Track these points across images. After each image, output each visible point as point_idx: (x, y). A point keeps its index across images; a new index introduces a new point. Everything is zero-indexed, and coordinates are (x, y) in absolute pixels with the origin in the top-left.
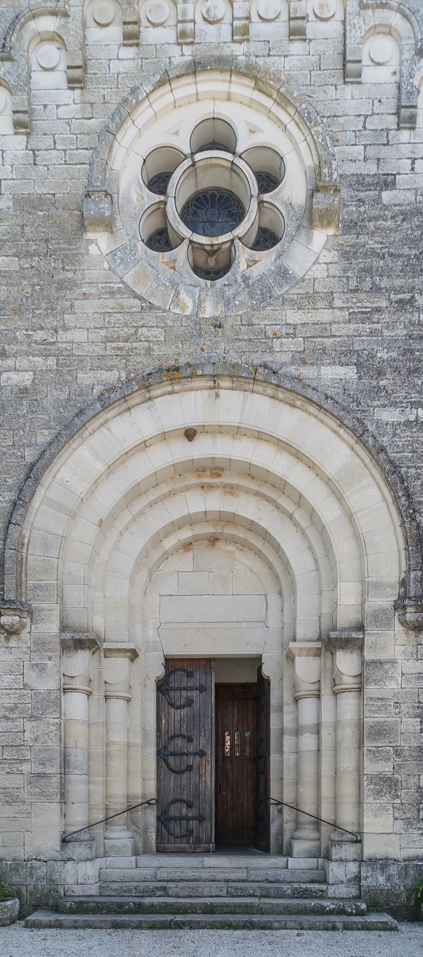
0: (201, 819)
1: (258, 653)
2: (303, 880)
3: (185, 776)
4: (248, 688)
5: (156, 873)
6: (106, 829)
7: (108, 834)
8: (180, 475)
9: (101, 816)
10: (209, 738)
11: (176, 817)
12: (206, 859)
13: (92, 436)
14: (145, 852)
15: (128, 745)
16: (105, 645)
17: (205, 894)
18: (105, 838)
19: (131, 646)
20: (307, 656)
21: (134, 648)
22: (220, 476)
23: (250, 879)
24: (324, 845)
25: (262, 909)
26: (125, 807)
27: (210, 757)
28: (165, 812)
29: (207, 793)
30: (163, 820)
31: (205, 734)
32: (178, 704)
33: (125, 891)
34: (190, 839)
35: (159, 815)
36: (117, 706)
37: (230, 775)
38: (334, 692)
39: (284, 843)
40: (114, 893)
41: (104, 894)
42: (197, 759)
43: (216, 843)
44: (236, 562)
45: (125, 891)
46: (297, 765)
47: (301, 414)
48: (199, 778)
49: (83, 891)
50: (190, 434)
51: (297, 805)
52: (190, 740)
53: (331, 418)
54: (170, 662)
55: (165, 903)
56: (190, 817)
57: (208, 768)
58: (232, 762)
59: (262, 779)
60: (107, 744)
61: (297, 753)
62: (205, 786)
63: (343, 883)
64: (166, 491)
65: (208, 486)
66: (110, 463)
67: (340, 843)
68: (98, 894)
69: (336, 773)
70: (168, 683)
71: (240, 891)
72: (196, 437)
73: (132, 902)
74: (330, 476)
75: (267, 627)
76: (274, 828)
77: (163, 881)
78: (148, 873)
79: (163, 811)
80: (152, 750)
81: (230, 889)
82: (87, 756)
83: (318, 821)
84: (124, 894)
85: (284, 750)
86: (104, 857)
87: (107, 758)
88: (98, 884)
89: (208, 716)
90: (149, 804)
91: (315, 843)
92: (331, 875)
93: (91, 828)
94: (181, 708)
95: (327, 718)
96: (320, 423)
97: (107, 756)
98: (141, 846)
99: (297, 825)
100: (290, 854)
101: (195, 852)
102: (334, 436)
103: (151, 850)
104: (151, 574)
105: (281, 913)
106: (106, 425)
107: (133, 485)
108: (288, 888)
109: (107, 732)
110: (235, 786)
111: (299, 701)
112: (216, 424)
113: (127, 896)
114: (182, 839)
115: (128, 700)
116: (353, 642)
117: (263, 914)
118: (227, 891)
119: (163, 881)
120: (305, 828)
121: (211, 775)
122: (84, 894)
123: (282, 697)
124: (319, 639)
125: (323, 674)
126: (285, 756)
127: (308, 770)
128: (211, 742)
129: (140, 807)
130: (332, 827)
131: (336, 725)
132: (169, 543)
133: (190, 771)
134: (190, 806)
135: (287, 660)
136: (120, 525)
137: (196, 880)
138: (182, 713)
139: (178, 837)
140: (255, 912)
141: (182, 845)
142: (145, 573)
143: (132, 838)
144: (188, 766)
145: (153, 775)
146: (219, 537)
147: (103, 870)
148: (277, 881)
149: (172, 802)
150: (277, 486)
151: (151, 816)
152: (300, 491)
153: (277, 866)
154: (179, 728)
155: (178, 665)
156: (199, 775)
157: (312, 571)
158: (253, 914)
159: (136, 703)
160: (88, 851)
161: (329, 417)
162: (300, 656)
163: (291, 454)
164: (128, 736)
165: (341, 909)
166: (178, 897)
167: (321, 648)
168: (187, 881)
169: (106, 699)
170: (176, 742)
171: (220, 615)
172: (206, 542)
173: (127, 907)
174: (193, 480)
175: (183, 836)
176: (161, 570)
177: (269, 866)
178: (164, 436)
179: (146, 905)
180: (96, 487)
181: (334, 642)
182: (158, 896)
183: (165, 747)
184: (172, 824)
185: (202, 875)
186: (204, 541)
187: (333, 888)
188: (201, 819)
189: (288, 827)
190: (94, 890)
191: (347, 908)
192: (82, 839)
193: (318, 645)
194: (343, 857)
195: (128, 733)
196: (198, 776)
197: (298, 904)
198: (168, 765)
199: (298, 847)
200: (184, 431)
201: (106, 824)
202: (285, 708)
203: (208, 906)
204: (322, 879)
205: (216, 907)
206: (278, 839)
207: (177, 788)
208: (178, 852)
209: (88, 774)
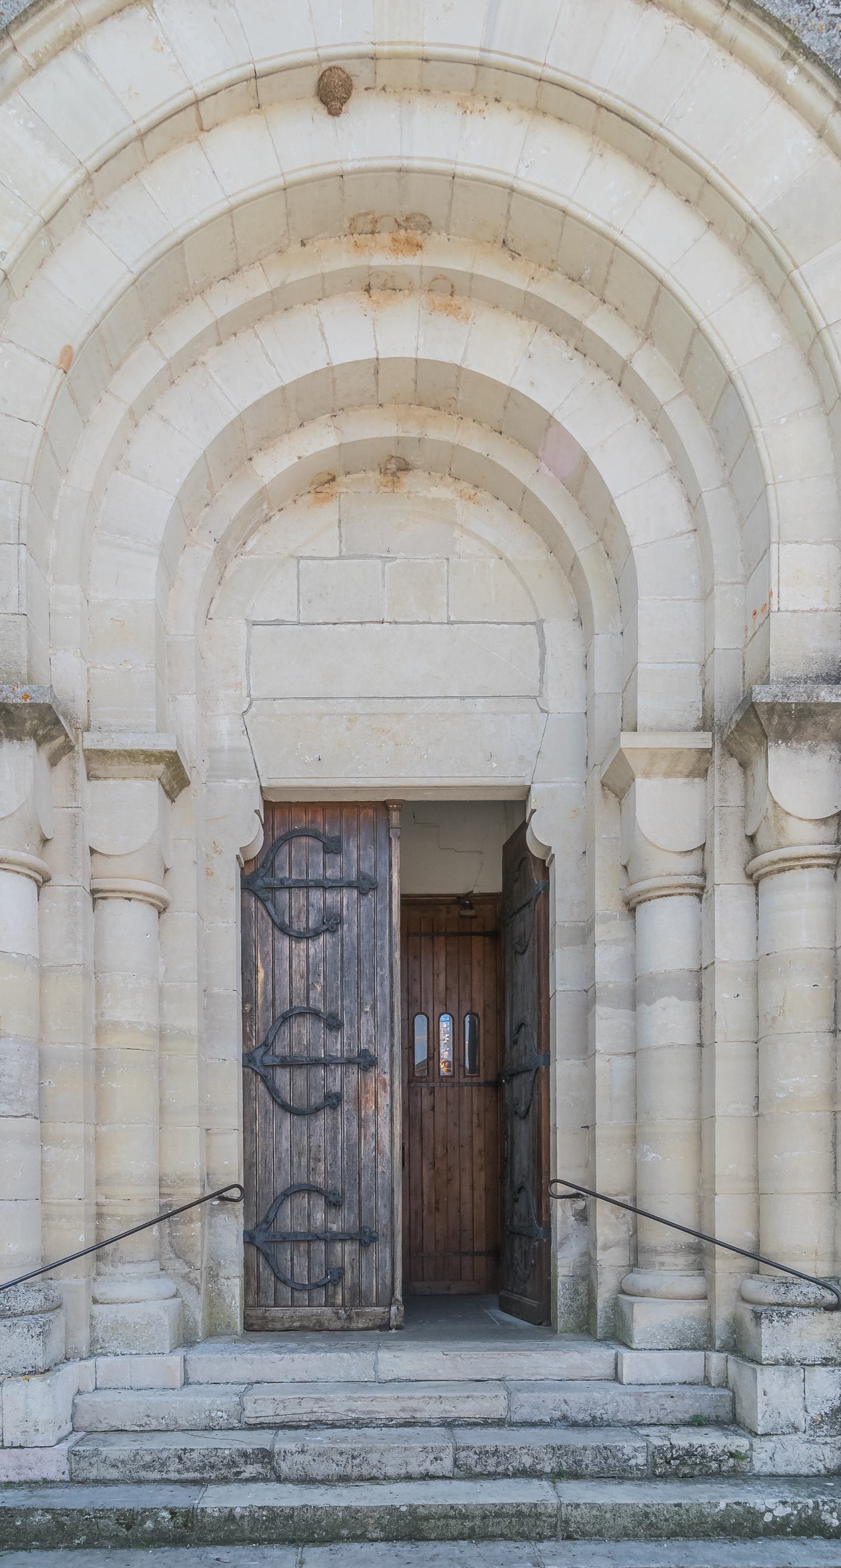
0: (364, 1238)
1: (517, 782)
2: (670, 1419)
3: (321, 1122)
4: (471, 907)
5: (240, 1403)
6: (99, 1274)
7: (102, 1289)
8: (303, 244)
9: (82, 1238)
10: (385, 1017)
11: (296, 1234)
12: (385, 1356)
13: (33, 80)
14: (212, 1334)
15: (162, 1035)
16: (90, 741)
17: (391, 1471)
18: (95, 1301)
19: (164, 744)
20: (668, 775)
21: (173, 748)
22: (420, 247)
23: (516, 1418)
24: (722, 1314)
25: (567, 1522)
26: (154, 1212)
27: (387, 1069)
28: (266, 1221)
29: (380, 1169)
30: (261, 1241)
31: (374, 1008)
32: (299, 925)
33: (146, 1467)
34: (335, 1293)
35: (250, 1228)
36: (128, 922)
37: (427, 1121)
38: (749, 876)
39: (600, 1305)
40: (114, 1474)
41: (83, 1475)
42: (354, 1075)
43: (405, 1302)
44: (457, 534)
45: (146, 1467)
46: (636, 1088)
47: (669, 23)
48: (359, 1126)
49: (20, 1467)
50: (333, 91)
51: (635, 1199)
52: (333, 1024)
53: (761, 33)
54: (277, 814)
55: (269, 1509)
56: (335, 1234)
57: (384, 1100)
58: (432, 1091)
59: (522, 1131)
60: (99, 1031)
61: (634, 1054)
62: (376, 1149)
63: (796, 1429)
64: (263, 289)
65: (384, 288)
66: (91, 165)
67: (784, 1310)
68: (66, 1477)
69: (757, 1107)
70: (272, 870)
71: (492, 1461)
72: (352, 104)
73: (165, 1508)
74: (754, 216)
75: (543, 711)
76: (565, 1263)
77: (261, 1426)
78: (216, 1403)
79: (261, 1218)
80: (230, 1050)
81: (463, 1454)
82: (35, 1062)
83: (702, 1245)
84: (143, 1474)
85: (598, 1046)
86: (92, 1354)
87: (98, 1070)
88: (65, 1446)
89: (382, 958)
90: (223, 1199)
91: (697, 1308)
92: (761, 1407)
93: (51, 1273)
94: (308, 938)
95: (731, 947)
96: (723, 55)
97: (98, 1065)
98: (199, 1317)
99: (637, 1255)
100: (618, 1334)
101: (348, 1329)
102: (764, 93)
103: (228, 1326)
104: (222, 558)
105: (627, 1535)
106: (77, 45)
107: (163, 247)
108: (636, 1450)
109: (99, 995)
110: (440, 1151)
111: (640, 909)
112: (412, 49)
113: (155, 1481)
114: (315, 1293)
115: (162, 908)
116: (819, 719)
117: (569, 1537)
118: (455, 1460)
119: (261, 1426)
120: (662, 1264)
121: (392, 1120)
122: (22, 1478)
123: (588, 901)
124: (705, 724)
125: (717, 825)
126: (600, 1063)
127: (671, 1099)
128: (392, 1029)
129: (197, 1209)
130: (748, 1262)
131: (759, 970)
132: (274, 465)
133: (334, 1107)
134: (334, 1203)
135: (605, 796)
136: (131, 384)
137: (358, 1424)
138: (312, 951)
139: (303, 1288)
140: (548, 1532)
141: (315, 1310)
142: (205, 550)
143: (175, 1296)
144: (327, 1096)
145: (234, 1120)
146: (411, 459)
147: (86, 1397)
148: (594, 1423)
149: (287, 1194)
150: (586, 274)
151: (229, 1232)
152: (660, 271)
153: (587, 1374)
154: (303, 993)
155: (302, 821)
156: (359, 1118)
157: (681, 534)
158: (541, 1538)
159: (183, 916)
160: (36, 1345)
161: (754, 28)
162: (647, 775)
163: (632, 159)
164: (161, 1009)
165: (809, 1518)
166: (307, 1481)
167: (710, 751)
168: (333, 1426)
169: (94, 900)
170: (295, 1030)
171: (413, 675)
172: (374, 476)
173: (149, 1524)
174: (340, 258)
175: (318, 1286)
176: (251, 552)
177: (565, 1374)
178: (254, 91)
179: (211, 1516)
180: (52, 250)
181: (763, 718)
182: (247, 1480)
183: (265, 1044)
184: (285, 1254)
185: (376, 1406)
186: (371, 474)
187: (769, 1444)
188: (364, 1238)
189: (610, 1261)
190: (53, 1465)
191: (826, 1517)
192: (19, 1306)
193: (704, 740)
194: (795, 1354)
195: (160, 1001)
196: (355, 1123)
197: (678, 1505)
198: (273, 1092)
199: (647, 1319)
200: (311, 78)
201: (99, 1258)
202: (600, 931)
203: (402, 1516)
204: (724, 1412)
205: (427, 1518)
206: (576, 1292)
207: (300, 1154)
208: (302, 1328)
209: (40, 1114)
